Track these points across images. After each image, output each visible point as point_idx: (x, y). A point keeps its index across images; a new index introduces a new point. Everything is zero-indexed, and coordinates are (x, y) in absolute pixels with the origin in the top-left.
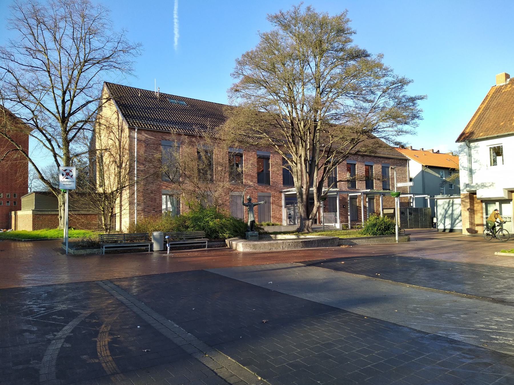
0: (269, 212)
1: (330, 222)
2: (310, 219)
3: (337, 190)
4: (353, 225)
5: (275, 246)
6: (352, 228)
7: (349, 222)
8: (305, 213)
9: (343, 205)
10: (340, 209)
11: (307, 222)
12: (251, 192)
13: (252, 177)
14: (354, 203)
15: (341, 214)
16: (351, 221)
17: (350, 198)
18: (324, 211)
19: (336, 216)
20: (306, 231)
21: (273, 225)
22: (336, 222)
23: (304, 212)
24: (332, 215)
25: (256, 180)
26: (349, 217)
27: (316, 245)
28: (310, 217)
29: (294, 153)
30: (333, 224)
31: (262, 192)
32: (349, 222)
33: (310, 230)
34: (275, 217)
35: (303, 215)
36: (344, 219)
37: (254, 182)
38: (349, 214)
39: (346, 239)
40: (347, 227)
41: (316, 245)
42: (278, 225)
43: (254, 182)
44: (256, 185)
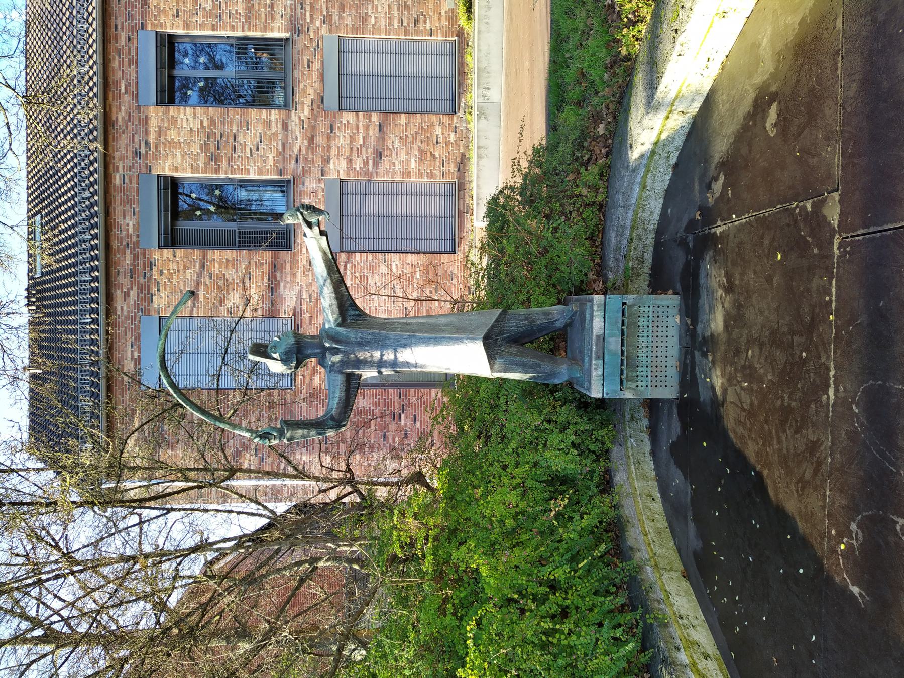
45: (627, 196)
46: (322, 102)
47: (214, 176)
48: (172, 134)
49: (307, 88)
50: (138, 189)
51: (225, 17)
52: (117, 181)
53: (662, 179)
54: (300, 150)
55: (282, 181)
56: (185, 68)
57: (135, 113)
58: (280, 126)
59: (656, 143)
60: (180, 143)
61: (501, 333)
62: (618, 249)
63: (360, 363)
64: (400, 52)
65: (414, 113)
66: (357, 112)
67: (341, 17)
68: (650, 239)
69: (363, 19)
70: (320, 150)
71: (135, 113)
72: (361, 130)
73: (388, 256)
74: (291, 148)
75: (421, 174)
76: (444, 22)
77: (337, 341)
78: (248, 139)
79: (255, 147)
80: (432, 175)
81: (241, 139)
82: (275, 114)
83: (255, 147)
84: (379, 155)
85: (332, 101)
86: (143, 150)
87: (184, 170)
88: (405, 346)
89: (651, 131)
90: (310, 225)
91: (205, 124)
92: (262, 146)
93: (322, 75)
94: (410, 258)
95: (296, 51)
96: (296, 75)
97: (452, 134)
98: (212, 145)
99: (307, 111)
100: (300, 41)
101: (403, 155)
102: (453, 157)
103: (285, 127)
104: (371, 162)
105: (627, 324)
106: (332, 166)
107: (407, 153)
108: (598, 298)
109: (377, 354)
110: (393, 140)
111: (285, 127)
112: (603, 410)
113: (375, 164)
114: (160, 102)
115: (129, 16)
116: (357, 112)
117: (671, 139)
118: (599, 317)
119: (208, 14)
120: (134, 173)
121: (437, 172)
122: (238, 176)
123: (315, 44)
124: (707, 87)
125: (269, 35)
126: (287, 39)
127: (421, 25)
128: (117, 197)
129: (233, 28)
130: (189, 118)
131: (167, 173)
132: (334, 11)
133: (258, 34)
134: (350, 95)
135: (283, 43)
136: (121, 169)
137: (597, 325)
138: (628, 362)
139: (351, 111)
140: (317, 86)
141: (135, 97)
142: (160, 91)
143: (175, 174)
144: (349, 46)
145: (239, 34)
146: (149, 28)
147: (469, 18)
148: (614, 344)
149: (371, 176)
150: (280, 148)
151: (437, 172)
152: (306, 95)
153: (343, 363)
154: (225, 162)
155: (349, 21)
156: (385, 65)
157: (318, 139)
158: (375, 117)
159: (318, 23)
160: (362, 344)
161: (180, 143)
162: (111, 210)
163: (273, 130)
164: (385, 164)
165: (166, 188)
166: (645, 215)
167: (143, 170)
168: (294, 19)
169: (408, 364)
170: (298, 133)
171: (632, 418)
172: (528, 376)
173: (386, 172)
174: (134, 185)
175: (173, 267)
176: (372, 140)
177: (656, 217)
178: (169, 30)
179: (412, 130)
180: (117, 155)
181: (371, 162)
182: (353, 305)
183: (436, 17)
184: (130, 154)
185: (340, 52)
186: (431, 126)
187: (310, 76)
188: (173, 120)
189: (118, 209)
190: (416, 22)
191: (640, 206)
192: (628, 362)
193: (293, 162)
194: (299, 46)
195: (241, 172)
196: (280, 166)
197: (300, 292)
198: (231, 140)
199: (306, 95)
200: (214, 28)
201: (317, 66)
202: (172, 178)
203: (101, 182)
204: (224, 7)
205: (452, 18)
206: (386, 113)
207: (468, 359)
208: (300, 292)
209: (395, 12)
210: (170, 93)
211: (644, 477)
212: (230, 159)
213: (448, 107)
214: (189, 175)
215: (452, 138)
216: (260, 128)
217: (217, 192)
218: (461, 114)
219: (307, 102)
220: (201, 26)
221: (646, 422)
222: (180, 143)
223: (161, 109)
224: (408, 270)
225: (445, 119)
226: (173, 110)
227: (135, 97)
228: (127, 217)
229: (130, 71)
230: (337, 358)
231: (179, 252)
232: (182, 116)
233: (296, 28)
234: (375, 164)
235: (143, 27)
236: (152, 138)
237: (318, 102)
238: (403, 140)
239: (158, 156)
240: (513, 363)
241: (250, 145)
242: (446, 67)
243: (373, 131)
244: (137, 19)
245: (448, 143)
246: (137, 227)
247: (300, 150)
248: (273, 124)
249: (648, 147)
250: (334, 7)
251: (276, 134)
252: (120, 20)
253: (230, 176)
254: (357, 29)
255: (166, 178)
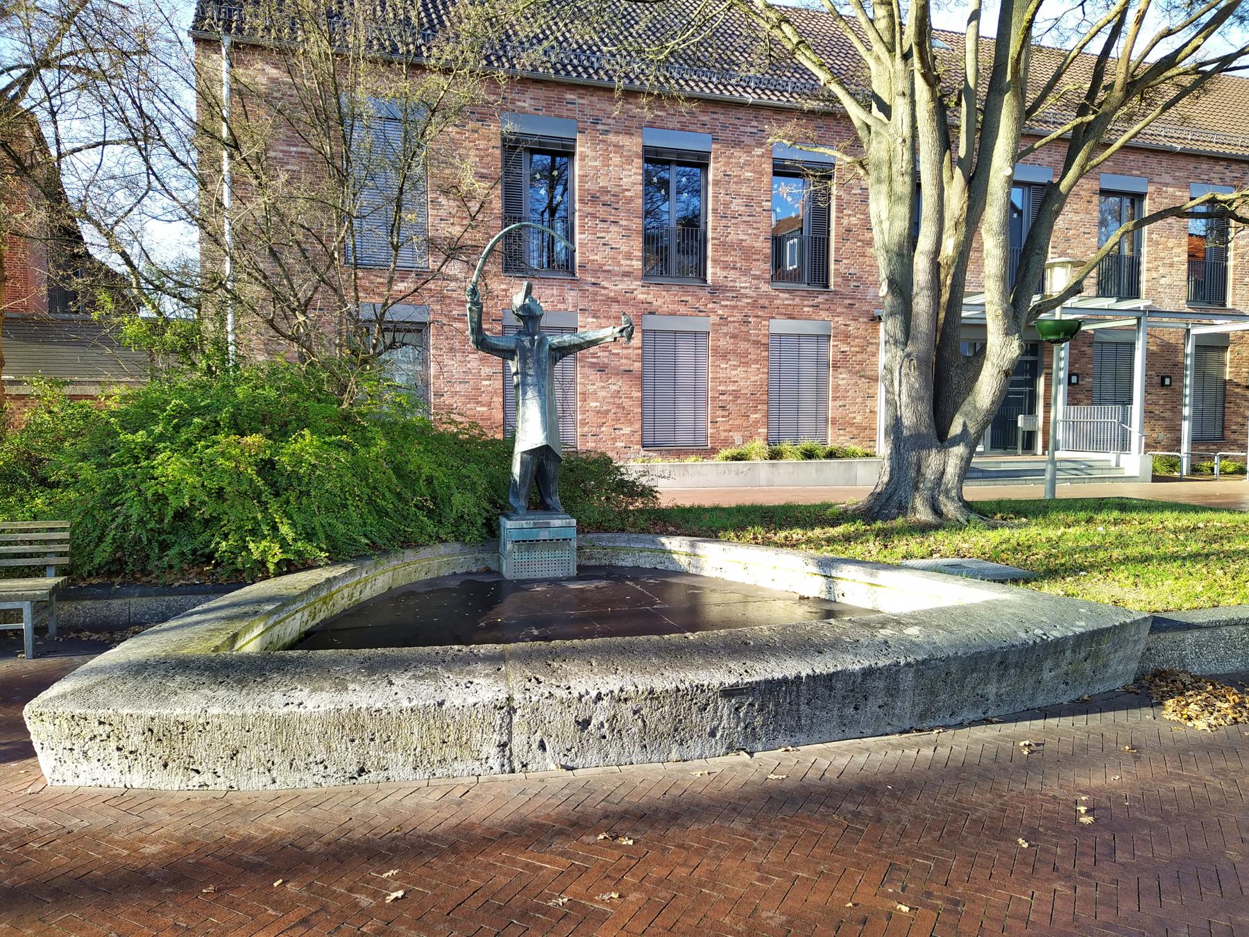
0: (820, 398)
1: (1096, 444)
2: (956, 441)
3: (1140, 304)
4: (1202, 458)
5: (413, 734)
6: (1195, 470)
7: (1185, 447)
8: (924, 407)
9: (1164, 376)
10: (1147, 392)
11: (933, 460)
12: (739, 317)
13: (748, 253)
14: (1212, 369)
15: (1149, 415)
16: (1195, 441)
17: (1198, 347)
18: (1072, 400)
19: (1126, 419)
20: (923, 514)
21: (831, 455)
22: (1124, 446)
23: (914, 399)
24: (1108, 415)
25: (763, 267)
26: (1186, 427)
27: (905, 705)
28: (956, 429)
29: (879, 49)
30: (1111, 457)
31: (791, 317)
32: (1185, 447)
33: (950, 509)
34: (843, 424)
35: (908, 419)
36: (1161, 435)
37: (756, 277)
38: (1186, 411)
39: (1214, 626)
40: (1174, 465)
41: (905, 705)
42: (854, 455)
43: (756, 277)
44: (765, 287)
45: (636, 540)
46: (651, 313)
47: (577, 198)
48: (616, 159)
49: (661, 298)
50: (561, 117)
51: (724, 222)
52: (570, 96)
53: (646, 562)
54: (605, 288)
55: (573, 267)
56: (673, 175)
57: (635, 123)
58: (627, 269)
59: (670, 552)
60: (606, 166)
61: (547, 459)
62: (599, 539)
63: (523, 360)
64: (697, 392)
65: (642, 406)
66: (642, 348)
67: (726, 334)
68: (605, 562)
69: (724, 356)
70: (604, 308)
71: (635, 123)
72: (625, 351)
73: (500, 377)
74: (609, 280)
75: (584, 412)
76: (723, 434)
77: (539, 345)
78: (613, 235)
79: (608, 244)
80: (584, 424)
81: (613, 228)
82: (638, 264)
83: (608, 244)
84: (602, 369)
85: (652, 323)
86: (600, 127)
87: (581, 167)
88: (539, 391)
89: (676, 545)
90: (621, 331)
91: (627, 194)
92: (608, 249)
93: (675, 314)
94: (498, 400)
95: (695, 289)
96: (674, 288)
97: (623, 444)
98: (607, 198)
99: (641, 297)
100: (704, 294)
101: (602, 394)
102: (601, 445)
103: (626, 274)
104: (594, 360)
105: (557, 543)
106: (590, 320)
107: (604, 398)
108: (574, 522)
109: (531, 372)
110: (617, 384)
111: (626, 274)
112: (492, 531)
113: (593, 365)
114: (646, 150)
115: (724, 127)
116: (642, 348)
117: (673, 561)
118: (561, 523)
119: (727, 205)
120: (578, 115)
121: (586, 429)
122: (577, 222)
123: (702, 308)
124: (704, 573)
125: (709, 263)
126: (705, 281)
127: (720, 413)
128: (553, 94)
129: (714, 229)
130: (631, 177)
131: (578, 150)
132: (731, 329)
133: (709, 253)
134: (659, 345)
135: (700, 272)
136: (581, 101)
137: (557, 523)
138: (529, 544)
139: (643, 341)
140: (665, 308)
141: (651, 125)
142: (657, 151)
143: (577, 157)
144: (701, 342)
145: (710, 235)
146: (714, 146)
147: (727, 458)
148: (544, 535)
149: (581, 361)
150: (605, 268)
151: (586, 429)
152: (657, 297)
153: (523, 349)
154: (590, 210)
155: (722, 343)
156: (685, 377)
157: (615, 308)
158: (638, 365)
159: (720, 312)
160: (538, 361)
161: (606, 166)
162: (540, 86)
163: (623, 262)
164: (593, 375)
165: (563, 146)
166: (622, 556)
167: (581, 125)
168: (724, 289)
169: (525, 393)
170: (620, 287)
171: (477, 560)
172: (518, 479)
173: (585, 376)
174: (565, 113)
175: (482, 144)
176: (615, 362)
177: (620, 563)
178: (712, 166)
179: (626, 403)
180: (595, 99)
181: (594, 360)
182: (564, 356)
183: (727, 427)
184: (597, 113)
185: (696, 333)
186: (631, 423)
187: (673, 302)
188: (630, 162)
189: (542, 93)
190: (723, 408)
191: (629, 551)
192: (529, 544)
193: (593, 280)
194: (701, 293)
195: (582, 226)
196: (589, 266)
197: (456, 280)
198: (612, 219)
199: (657, 297)
200: (715, 210)
201: (682, 309)
202: (573, 154)
203: (568, 80)
204: (733, 221)
205: (727, 443)
206: (642, 377)
207: (531, 434)
208: (456, 280)
209: (731, 388)
210: (654, 158)
211: (440, 568)
212: (594, 216)
213: (649, 440)
214: (577, 172)
215: (620, 444)
216: (624, 248)
217: (538, 176)
218: (642, 452)
219: (650, 298)
220: (715, 197)
221: (474, 570)
222: (608, 166)
223: (640, 150)
224: (484, 398)
225: (637, 437)
226: (639, 162)
227: (651, 125)
228: (532, 102)
229: (674, 123)
230: (527, 344)
231: (498, 152)
232: (634, 170)
233: (716, 290)
234: (593, 365)
235: (715, 140)
236: (612, 138)
237: (652, 309)
238: (617, 394)
239: (595, 142)
240: (527, 467)
241: (608, 237)
242: (684, 438)
243: (624, 364)
244: (722, 135)
245: (614, 440)
246: (522, 111)
247: (605, 288)
248: (628, 262)
249: (668, 547)
250: (735, 328)
251: (619, 265)
252: (721, 117)
253: (577, 214)
254: (715, 350)
255: (574, 147)
